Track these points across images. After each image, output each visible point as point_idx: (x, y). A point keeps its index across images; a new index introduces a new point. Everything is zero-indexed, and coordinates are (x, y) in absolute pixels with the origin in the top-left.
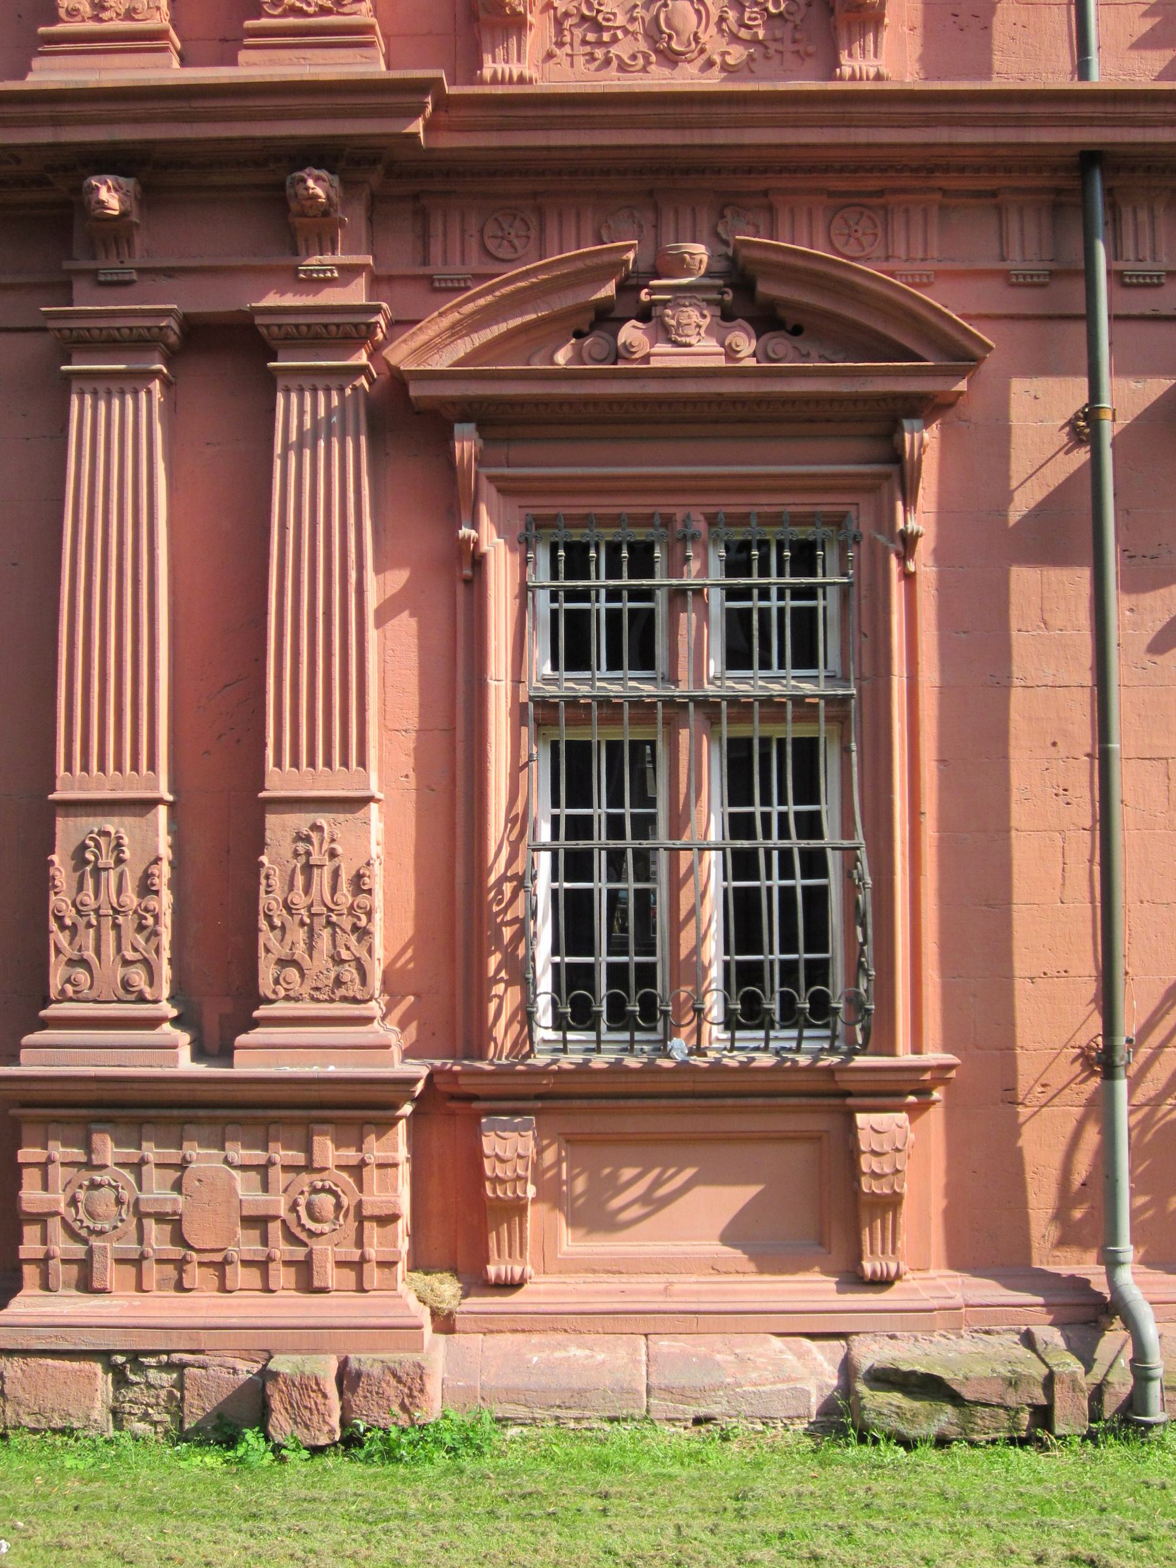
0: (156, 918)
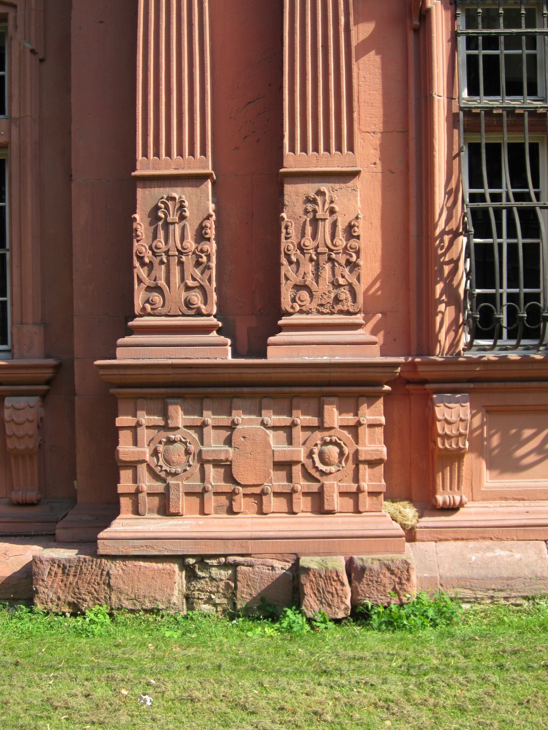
0: (209, 257)
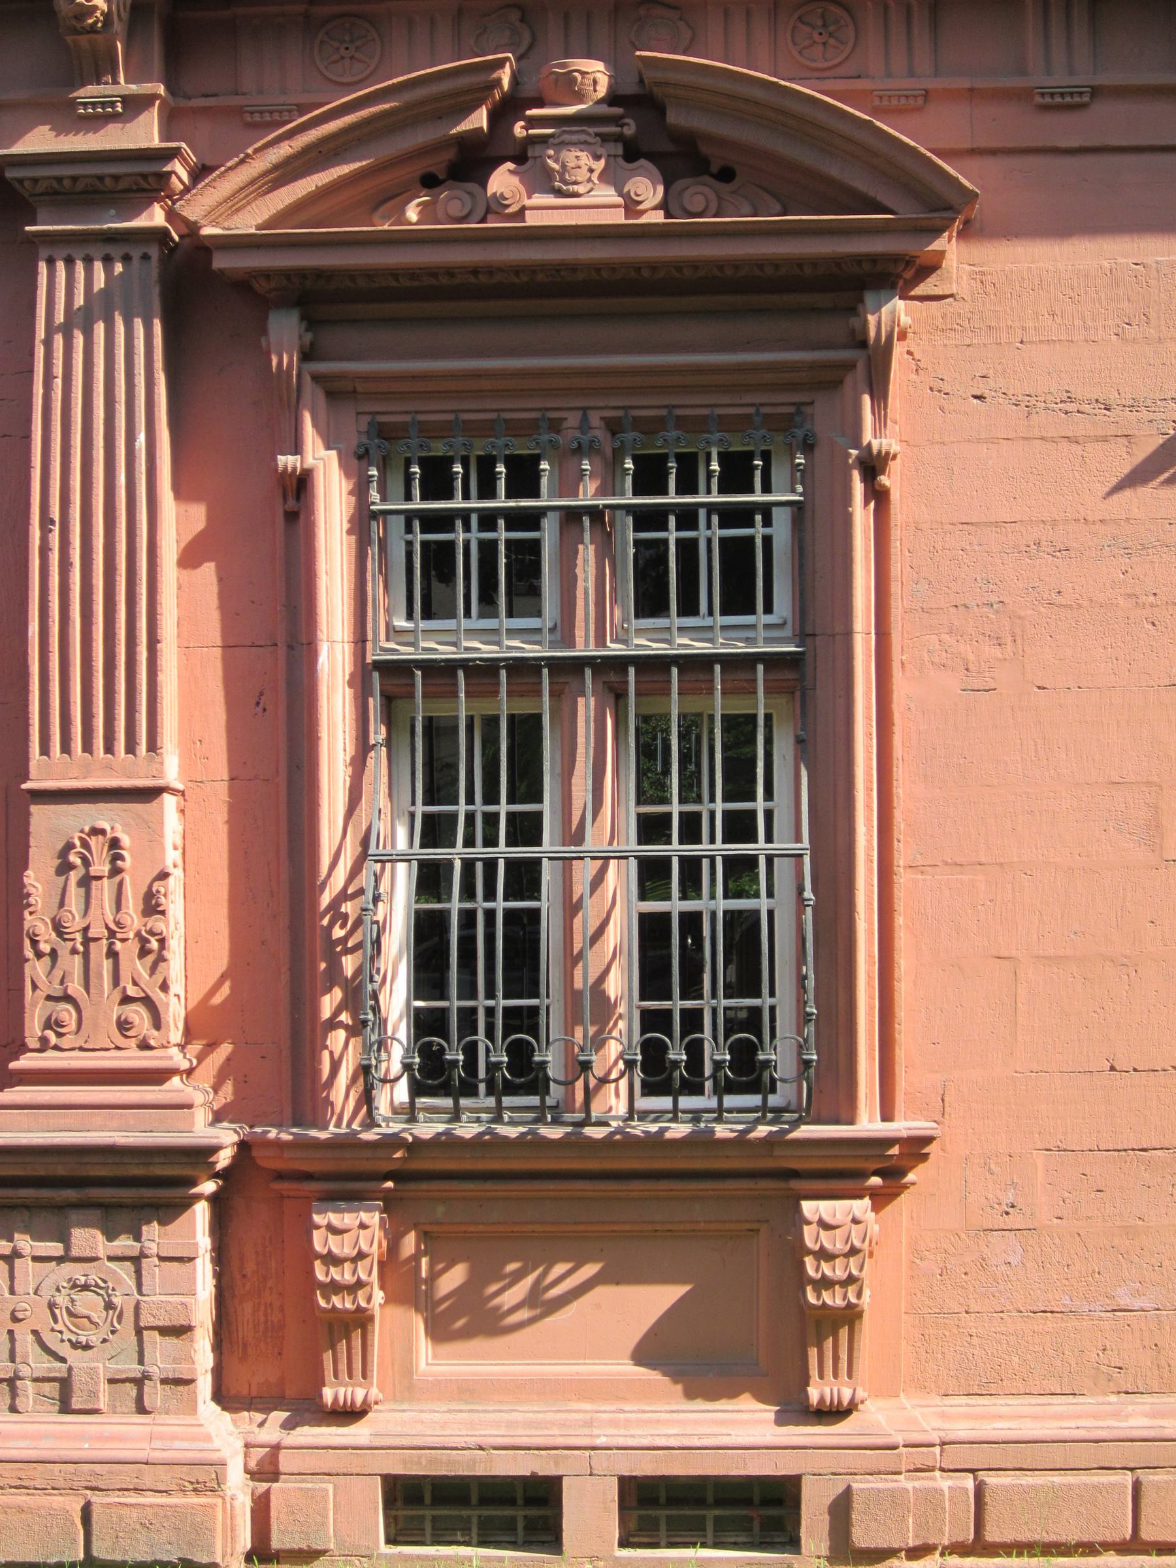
0: (162, 942)
